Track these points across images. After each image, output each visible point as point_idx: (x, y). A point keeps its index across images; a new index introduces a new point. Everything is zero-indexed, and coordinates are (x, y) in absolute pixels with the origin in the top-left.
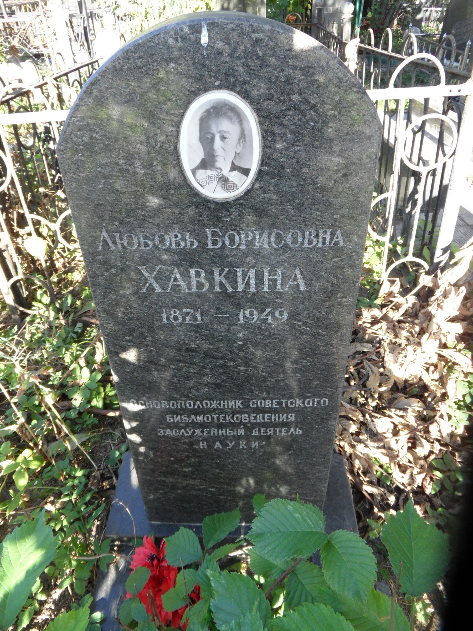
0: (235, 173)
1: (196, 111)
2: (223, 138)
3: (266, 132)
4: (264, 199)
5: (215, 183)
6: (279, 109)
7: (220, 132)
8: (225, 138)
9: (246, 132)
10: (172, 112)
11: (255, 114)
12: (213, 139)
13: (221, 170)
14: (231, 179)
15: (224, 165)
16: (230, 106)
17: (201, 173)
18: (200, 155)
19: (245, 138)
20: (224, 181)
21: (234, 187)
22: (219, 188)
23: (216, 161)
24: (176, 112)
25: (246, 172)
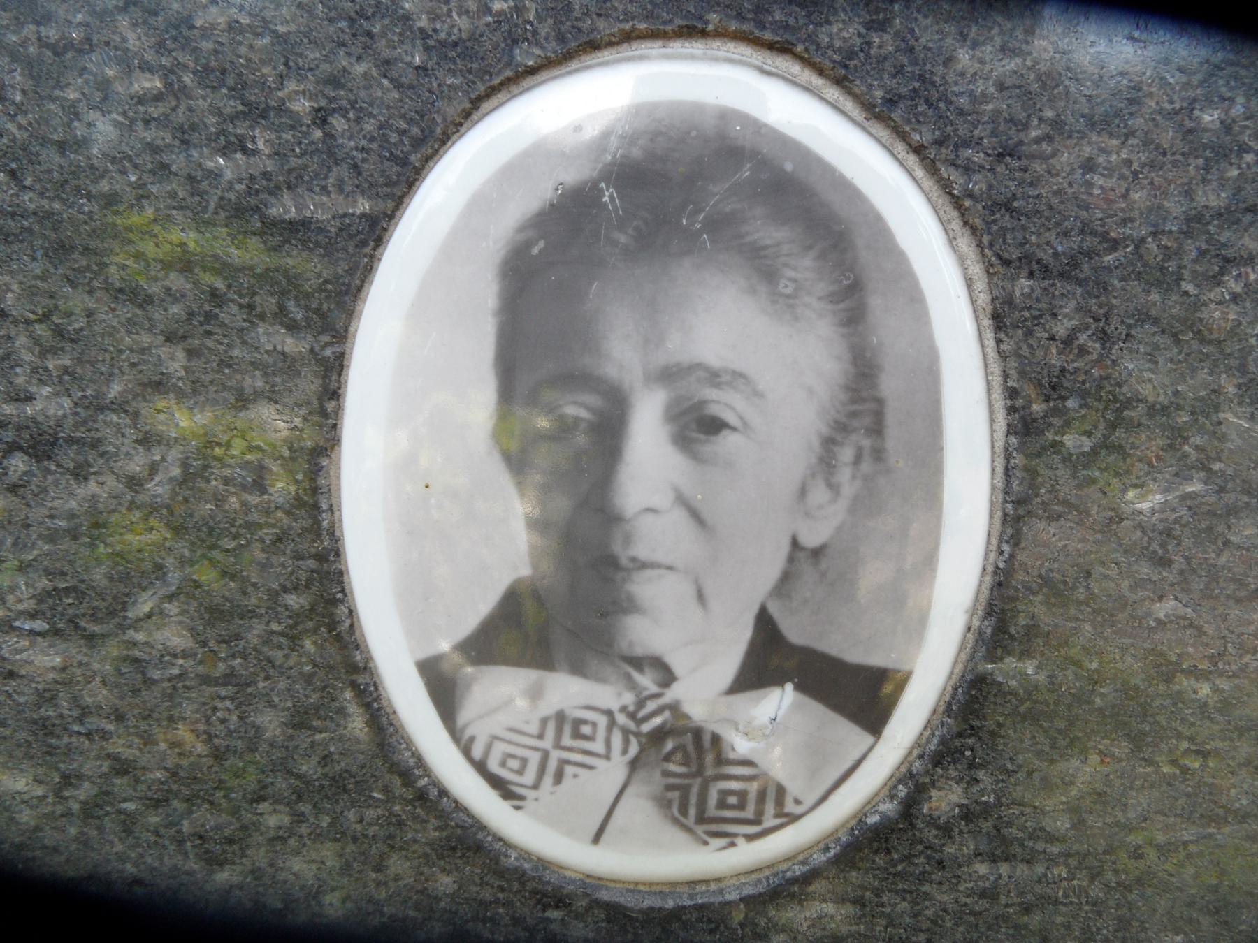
0: (780, 701)
1: (479, 205)
2: (697, 427)
3: (1054, 388)
4: (989, 894)
5: (612, 772)
6: (1175, 206)
7: (668, 375)
8: (714, 426)
9: (890, 385)
10: (285, 208)
11: (966, 243)
12: (609, 431)
13: (667, 676)
14: (741, 746)
15: (693, 642)
16: (761, 162)
17: (507, 699)
18: (504, 543)
19: (877, 430)
20: (688, 770)
21: (770, 804)
22: (639, 810)
23: (630, 606)
24: (317, 207)
25: (861, 695)
